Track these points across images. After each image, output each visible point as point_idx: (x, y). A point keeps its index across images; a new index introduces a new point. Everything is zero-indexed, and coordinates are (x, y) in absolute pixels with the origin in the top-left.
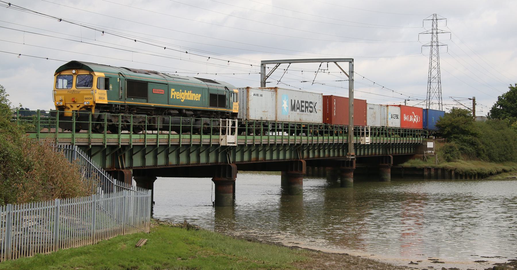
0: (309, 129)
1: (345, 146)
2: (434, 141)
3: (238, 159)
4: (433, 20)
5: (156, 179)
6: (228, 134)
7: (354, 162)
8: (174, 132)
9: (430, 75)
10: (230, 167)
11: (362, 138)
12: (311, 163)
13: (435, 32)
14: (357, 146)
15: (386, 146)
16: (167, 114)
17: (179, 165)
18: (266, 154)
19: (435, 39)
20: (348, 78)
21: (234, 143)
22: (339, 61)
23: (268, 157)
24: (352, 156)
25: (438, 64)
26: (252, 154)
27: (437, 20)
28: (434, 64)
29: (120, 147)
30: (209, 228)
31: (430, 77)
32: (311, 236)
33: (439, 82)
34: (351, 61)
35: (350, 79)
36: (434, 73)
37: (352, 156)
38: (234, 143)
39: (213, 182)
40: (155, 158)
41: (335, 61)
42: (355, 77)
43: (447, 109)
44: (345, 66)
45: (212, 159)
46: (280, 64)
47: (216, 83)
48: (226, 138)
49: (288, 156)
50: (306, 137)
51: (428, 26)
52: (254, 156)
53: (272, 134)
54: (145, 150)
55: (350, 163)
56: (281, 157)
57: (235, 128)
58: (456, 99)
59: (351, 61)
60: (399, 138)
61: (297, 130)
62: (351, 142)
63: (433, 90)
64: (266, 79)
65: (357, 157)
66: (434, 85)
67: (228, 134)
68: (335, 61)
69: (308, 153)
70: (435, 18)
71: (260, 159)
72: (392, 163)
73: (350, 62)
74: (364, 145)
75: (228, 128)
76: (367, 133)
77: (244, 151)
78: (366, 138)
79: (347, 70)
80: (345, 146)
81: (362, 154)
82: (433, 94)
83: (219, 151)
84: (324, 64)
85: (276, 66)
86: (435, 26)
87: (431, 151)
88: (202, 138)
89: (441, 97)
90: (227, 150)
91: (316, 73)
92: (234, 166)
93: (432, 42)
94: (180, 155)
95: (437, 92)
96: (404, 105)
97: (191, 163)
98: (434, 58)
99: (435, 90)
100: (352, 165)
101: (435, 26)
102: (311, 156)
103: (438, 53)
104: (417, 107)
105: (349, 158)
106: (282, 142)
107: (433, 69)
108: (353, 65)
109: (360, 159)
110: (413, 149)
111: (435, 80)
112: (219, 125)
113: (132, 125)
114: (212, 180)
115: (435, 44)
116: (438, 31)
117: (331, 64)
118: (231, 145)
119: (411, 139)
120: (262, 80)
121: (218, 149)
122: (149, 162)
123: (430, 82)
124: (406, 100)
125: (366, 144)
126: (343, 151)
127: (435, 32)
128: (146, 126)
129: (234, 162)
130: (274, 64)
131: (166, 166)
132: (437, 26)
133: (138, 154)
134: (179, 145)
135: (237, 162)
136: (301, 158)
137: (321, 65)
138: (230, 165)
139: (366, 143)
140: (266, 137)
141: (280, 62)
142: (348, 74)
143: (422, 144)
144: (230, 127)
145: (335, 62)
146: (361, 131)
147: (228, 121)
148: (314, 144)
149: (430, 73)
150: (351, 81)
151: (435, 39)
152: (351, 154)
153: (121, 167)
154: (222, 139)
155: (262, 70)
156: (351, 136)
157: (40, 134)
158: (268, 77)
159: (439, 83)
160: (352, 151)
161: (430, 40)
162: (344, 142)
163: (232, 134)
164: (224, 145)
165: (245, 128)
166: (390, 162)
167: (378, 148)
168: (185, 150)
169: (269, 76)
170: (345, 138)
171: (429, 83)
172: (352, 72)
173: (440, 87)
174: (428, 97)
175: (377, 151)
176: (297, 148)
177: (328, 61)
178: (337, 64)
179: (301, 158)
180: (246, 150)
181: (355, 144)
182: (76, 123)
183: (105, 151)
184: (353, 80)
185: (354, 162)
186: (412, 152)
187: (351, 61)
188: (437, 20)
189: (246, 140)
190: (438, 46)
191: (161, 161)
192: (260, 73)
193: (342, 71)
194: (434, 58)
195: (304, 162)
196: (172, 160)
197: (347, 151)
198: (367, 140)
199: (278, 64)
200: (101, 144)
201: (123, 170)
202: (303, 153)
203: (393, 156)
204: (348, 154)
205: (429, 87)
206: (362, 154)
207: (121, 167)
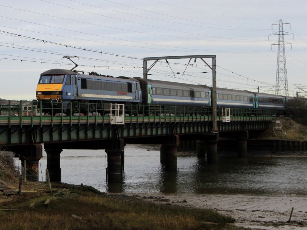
0: (227, 111)
1: (210, 124)
2: (281, 119)
3: (125, 134)
4: (279, 24)
5: (62, 150)
6: (117, 116)
7: (218, 136)
8: (82, 114)
9: (278, 67)
10: (119, 141)
11: (223, 117)
12: (183, 137)
13: (281, 33)
14: (220, 123)
15: (242, 123)
16: (88, 102)
17: (141, 136)
18: (147, 130)
19: (281, 39)
20: (211, 71)
21: (122, 122)
22: (205, 57)
23: (149, 133)
24: (216, 131)
25: (284, 58)
26: (124, 131)
27: (282, 24)
28: (281, 59)
29: (22, 127)
30: (103, 189)
31: (278, 68)
32: (164, 199)
33: (285, 73)
34: (214, 57)
35: (214, 71)
36: (282, 65)
37: (216, 131)
38: (122, 122)
39: (106, 153)
40: (69, 134)
41: (201, 57)
42: (218, 69)
43: (292, 94)
44: (209, 61)
45: (105, 135)
46: (158, 60)
47: (98, 75)
48: (115, 119)
49: (164, 131)
50: (130, 117)
51: (276, 28)
52: (143, 132)
53: (41, 114)
54: (52, 129)
55: (215, 137)
56: (159, 133)
57: (229, 113)
58: (298, 86)
59: (214, 57)
60: (174, 117)
61: (145, 111)
62: (215, 120)
63: (281, 79)
64: (148, 72)
65: (220, 132)
66: (282, 75)
67: (117, 116)
68: (201, 57)
69: (181, 130)
70: (281, 23)
71: (142, 135)
72: (248, 136)
73: (213, 58)
74: (225, 123)
75: (117, 111)
76: (121, 113)
77: (136, 128)
78: (227, 117)
79: (211, 64)
80: (210, 124)
81: (224, 130)
82: (281, 82)
83: (110, 129)
84: (193, 59)
85: (155, 62)
86: (281, 29)
87: (278, 127)
88: (72, 119)
89: (287, 84)
90: (116, 127)
91: (187, 65)
92: (122, 140)
93: (279, 42)
94: (53, 133)
95: (284, 80)
96: (258, 92)
97: (88, 138)
98: (281, 54)
99: (283, 79)
100: (216, 138)
101: (281, 29)
102: (183, 132)
103: (284, 50)
104: (267, 93)
105: (214, 133)
106: (160, 121)
107: (281, 62)
108: (215, 60)
109: (222, 134)
110: (265, 125)
111: (282, 72)
112: (70, 108)
113: (53, 110)
114: (105, 151)
115: (281, 43)
116: (284, 33)
117: (198, 60)
118: (120, 124)
119: (265, 117)
120: (144, 73)
121: (110, 127)
122: (56, 137)
123: (278, 72)
124: (258, 87)
125: (227, 122)
126: (209, 128)
127: (281, 33)
128: (62, 110)
129: (122, 137)
130: (153, 60)
131: (8, 145)
132: (283, 29)
133: (56, 131)
134: (78, 124)
135: (125, 137)
136: (175, 133)
137: (190, 60)
138: (119, 140)
139: (227, 121)
140: (158, 117)
141: (158, 58)
142: (212, 67)
143: (271, 121)
144: (118, 110)
145: (201, 58)
146: (223, 112)
147: (117, 105)
148: (194, 122)
149: (278, 65)
150: (214, 73)
151: (281, 39)
152: (215, 130)
153: (33, 142)
154: (112, 120)
155: (144, 64)
156: (214, 116)
157: (42, 117)
158: (149, 70)
159: (286, 74)
160: (216, 128)
161: (278, 40)
162: (209, 121)
163: (120, 116)
164: (225, 121)
165: (142, 111)
166: (246, 136)
167: (183, 126)
168: (75, 128)
169: (150, 69)
170: (210, 117)
171: (278, 74)
172: (214, 65)
173: (286, 76)
174: (277, 85)
175: (236, 127)
176: (172, 126)
177: (195, 57)
178: (203, 60)
179: (175, 133)
180: (55, 129)
181: (218, 122)
182: (54, 110)
183: (21, 130)
184: (215, 72)
185: (218, 136)
186: (111, 136)
187: (214, 57)
188: (282, 24)
189: (175, 119)
190: (284, 44)
191: (65, 137)
192: (143, 67)
193: (206, 65)
194: (281, 54)
195: (247, 132)
196: (74, 136)
197: (212, 127)
198: (228, 119)
199: (157, 60)
200: (18, 125)
201: (35, 145)
202: (177, 130)
203: (248, 131)
204: (212, 130)
205: (277, 76)
206: (224, 130)
207: (33, 142)
